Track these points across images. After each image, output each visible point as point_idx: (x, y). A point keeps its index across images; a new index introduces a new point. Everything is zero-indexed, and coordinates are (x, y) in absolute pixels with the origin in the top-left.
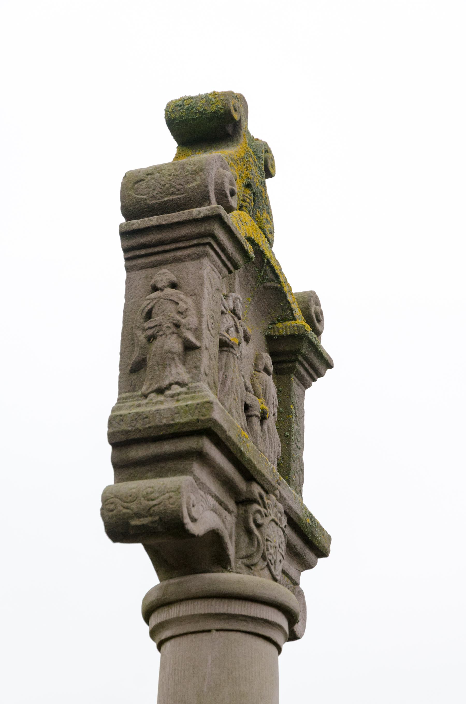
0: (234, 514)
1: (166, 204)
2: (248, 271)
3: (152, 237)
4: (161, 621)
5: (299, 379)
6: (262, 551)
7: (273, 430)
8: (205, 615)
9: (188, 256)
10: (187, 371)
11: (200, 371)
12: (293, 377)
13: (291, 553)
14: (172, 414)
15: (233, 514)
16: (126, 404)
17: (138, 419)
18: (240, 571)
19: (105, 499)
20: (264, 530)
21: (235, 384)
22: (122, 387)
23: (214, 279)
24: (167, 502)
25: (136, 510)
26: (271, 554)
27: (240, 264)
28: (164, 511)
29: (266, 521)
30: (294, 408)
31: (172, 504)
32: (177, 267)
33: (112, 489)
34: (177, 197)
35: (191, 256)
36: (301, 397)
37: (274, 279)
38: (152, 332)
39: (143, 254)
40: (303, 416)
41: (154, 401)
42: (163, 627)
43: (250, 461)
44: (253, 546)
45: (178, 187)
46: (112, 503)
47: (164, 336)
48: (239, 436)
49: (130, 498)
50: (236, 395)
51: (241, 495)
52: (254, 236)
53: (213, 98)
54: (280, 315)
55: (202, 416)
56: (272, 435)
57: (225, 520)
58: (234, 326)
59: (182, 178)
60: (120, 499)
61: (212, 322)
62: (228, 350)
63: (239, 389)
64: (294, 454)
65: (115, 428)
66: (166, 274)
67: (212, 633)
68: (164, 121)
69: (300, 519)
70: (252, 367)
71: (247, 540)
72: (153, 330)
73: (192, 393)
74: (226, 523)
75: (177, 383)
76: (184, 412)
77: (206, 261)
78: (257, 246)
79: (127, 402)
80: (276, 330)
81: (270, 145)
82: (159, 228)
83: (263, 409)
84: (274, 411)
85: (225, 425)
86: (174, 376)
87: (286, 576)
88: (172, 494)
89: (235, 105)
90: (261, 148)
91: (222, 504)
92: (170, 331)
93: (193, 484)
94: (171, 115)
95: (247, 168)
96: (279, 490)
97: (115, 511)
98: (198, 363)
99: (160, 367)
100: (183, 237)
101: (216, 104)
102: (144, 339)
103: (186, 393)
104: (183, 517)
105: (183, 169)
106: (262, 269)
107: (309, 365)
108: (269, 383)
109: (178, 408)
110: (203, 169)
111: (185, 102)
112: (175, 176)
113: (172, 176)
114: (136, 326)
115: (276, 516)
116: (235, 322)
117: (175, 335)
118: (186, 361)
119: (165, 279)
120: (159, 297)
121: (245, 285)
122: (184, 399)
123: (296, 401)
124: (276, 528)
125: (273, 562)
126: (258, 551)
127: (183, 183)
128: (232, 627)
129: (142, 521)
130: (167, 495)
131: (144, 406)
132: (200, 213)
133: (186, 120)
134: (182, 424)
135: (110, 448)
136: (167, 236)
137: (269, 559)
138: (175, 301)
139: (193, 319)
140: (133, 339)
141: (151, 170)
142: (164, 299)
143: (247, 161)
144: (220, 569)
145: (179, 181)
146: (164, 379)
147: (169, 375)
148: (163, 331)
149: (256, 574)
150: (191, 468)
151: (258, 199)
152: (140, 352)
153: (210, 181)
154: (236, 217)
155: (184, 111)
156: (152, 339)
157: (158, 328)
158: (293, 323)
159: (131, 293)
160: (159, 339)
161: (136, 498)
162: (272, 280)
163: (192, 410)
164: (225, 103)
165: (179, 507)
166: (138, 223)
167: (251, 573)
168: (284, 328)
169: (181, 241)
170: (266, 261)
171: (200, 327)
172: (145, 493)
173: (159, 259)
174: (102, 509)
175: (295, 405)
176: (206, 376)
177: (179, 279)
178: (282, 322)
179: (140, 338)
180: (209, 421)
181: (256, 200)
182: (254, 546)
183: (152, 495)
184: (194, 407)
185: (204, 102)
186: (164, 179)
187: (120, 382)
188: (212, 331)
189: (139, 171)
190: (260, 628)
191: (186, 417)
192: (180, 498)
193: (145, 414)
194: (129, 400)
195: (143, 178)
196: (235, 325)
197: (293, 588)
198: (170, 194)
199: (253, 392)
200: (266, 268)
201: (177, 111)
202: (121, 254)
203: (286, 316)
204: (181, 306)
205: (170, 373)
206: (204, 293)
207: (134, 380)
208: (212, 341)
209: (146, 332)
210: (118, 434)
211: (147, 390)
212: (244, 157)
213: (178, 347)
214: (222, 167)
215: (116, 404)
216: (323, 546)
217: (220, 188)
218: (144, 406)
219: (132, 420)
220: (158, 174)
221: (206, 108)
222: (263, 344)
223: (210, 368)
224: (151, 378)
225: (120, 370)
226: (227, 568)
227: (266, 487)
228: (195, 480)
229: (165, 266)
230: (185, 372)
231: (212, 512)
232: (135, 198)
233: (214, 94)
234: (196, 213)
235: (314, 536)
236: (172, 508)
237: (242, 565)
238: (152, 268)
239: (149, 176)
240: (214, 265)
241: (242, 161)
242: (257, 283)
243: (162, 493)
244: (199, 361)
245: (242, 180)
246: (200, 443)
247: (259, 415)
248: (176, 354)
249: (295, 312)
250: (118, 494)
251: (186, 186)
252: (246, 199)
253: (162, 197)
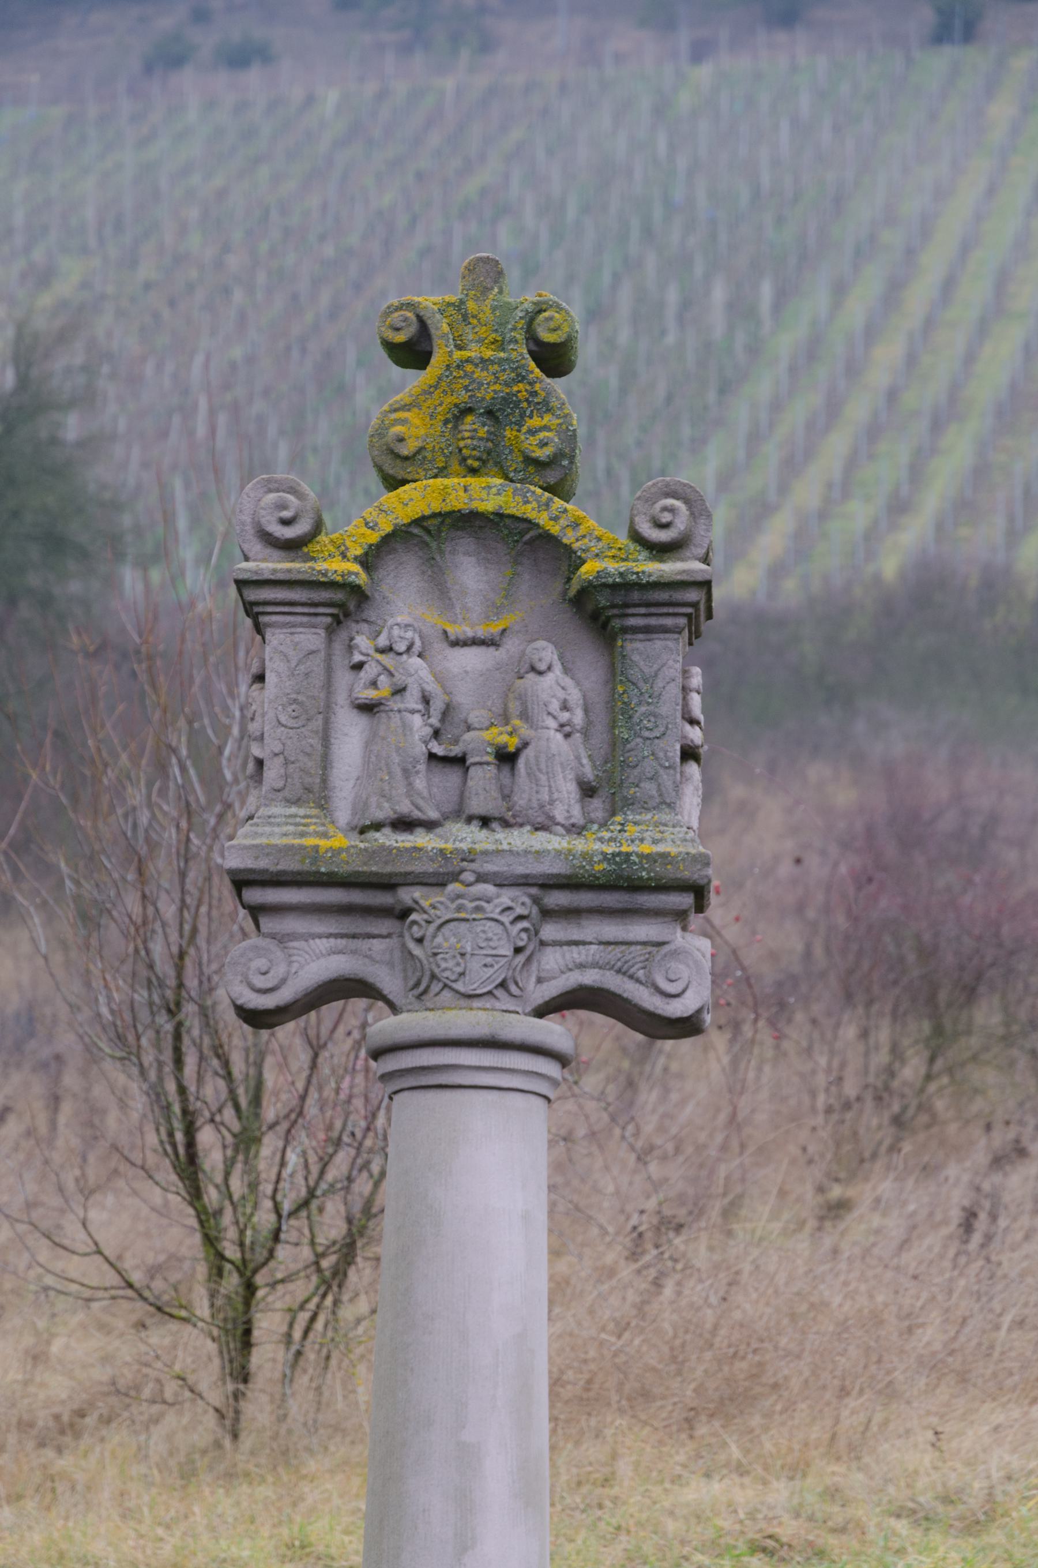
37: (529, 526)
162: (529, 529)
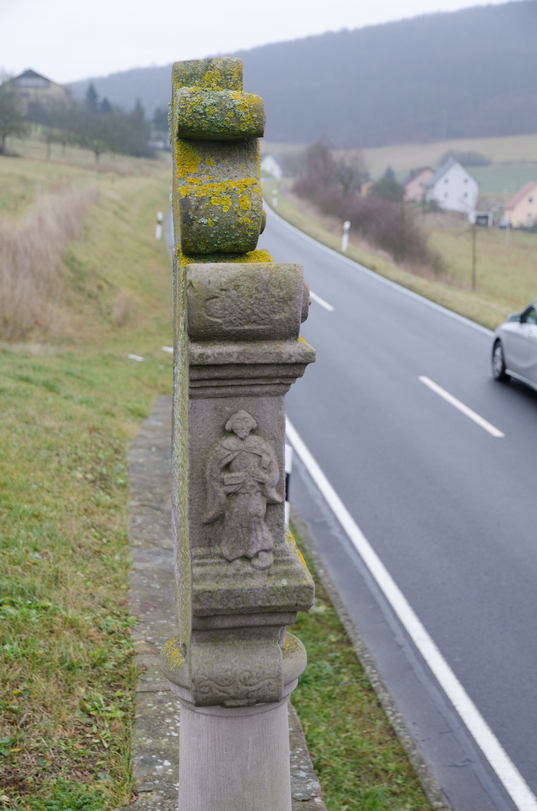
24: (267, 689)
31: (273, 691)
46: (206, 686)
55: (302, 601)
60: (215, 683)
66: (246, 420)
72: (236, 487)
88: (272, 681)
92: (255, 490)
99: (244, 529)
127: (268, 312)
130: (266, 681)
142: (247, 452)
145: (263, 307)
159: (197, 427)
164: (259, 124)
172: (243, 678)
185: (232, 116)
186: (244, 301)
193: (237, 593)
195: (217, 295)
205: (256, 538)
232: (208, 320)
239: (224, 293)
251: (271, 316)
253: (241, 324)
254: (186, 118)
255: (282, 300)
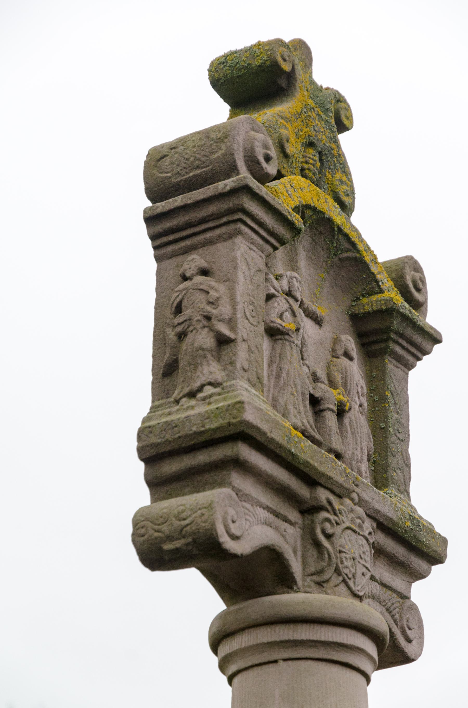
0: (299, 526)
1: (191, 180)
2: (316, 243)
3: (179, 219)
4: (225, 654)
5: (397, 361)
6: (335, 565)
7: (356, 423)
8: (268, 643)
9: (219, 236)
10: (222, 368)
11: (235, 367)
12: (387, 359)
13: (391, 563)
14: (202, 419)
15: (297, 526)
16: (156, 413)
17: (167, 428)
18: (309, 590)
19: (137, 523)
20: (335, 541)
21: (293, 376)
22: (155, 394)
23: (253, 259)
24: (199, 520)
25: (167, 532)
26: (347, 567)
27: (286, 238)
28: (197, 530)
29: (338, 530)
30: (392, 394)
31: (205, 522)
32: (209, 251)
33: (144, 511)
34: (202, 170)
35: (222, 236)
36: (402, 381)
37: (351, 248)
38: (181, 328)
39: (171, 240)
40: (407, 403)
41: (185, 407)
42: (228, 661)
43: (307, 463)
44: (323, 560)
45: (203, 159)
46: (142, 527)
47: (194, 332)
48: (287, 436)
49: (161, 519)
50: (294, 389)
51: (305, 502)
52: (313, 202)
53: (257, 50)
54: (364, 289)
55: (234, 418)
56: (356, 429)
57: (284, 533)
58: (290, 310)
59: (207, 149)
60: (151, 522)
61: (251, 309)
62: (283, 338)
63: (299, 382)
64: (393, 448)
65: (144, 441)
66: (195, 260)
67: (279, 663)
68: (208, 82)
69: (394, 523)
70: (329, 352)
71: (315, 553)
72: (183, 325)
73: (225, 393)
74: (287, 537)
75: (210, 384)
76: (214, 417)
77: (239, 240)
78: (321, 213)
79: (158, 411)
80: (360, 306)
81: (343, 93)
82: (185, 208)
83: (340, 401)
84: (360, 401)
85: (265, 426)
86: (206, 375)
87: (389, 589)
88: (204, 511)
89: (282, 54)
90: (329, 99)
91: (279, 515)
92: (201, 325)
93: (231, 497)
94: (214, 75)
95: (307, 124)
96: (356, 493)
97: (146, 536)
98: (234, 358)
99: (191, 367)
100: (211, 215)
101: (261, 56)
102: (174, 337)
103: (219, 394)
104: (217, 536)
105: (208, 137)
106: (334, 239)
107: (407, 342)
108: (350, 370)
109: (209, 412)
110: (228, 136)
111: (228, 58)
112: (199, 146)
113: (196, 148)
114: (166, 323)
115: (352, 521)
116: (290, 305)
117: (206, 329)
118: (221, 357)
119: (194, 265)
120: (187, 288)
121: (315, 260)
122: (216, 401)
123: (395, 386)
124: (354, 536)
125: (350, 576)
126: (329, 564)
127: (207, 154)
128: (300, 655)
129: (176, 544)
130: (199, 512)
131: (175, 413)
132: (226, 186)
133: (231, 78)
134: (213, 429)
135: (142, 465)
136: (194, 217)
137: (345, 574)
138: (205, 289)
139: (226, 309)
140: (164, 338)
141: (175, 143)
142: (194, 289)
143: (305, 116)
144: (286, 589)
145: (204, 152)
146: (195, 381)
147: (201, 376)
148: (193, 325)
149: (329, 591)
150: (229, 478)
151: (327, 158)
152: (171, 352)
153: (236, 149)
154: (284, 184)
155: (228, 68)
156: (183, 336)
157: (187, 323)
158: (380, 296)
160: (190, 335)
161: (168, 519)
162: (349, 250)
163: (223, 413)
164: (271, 54)
165: (212, 525)
166: (162, 206)
167: (322, 590)
168: (370, 303)
169: (209, 221)
170: (336, 229)
171: (234, 316)
172: (177, 513)
173: (189, 244)
174: (133, 535)
175: (392, 391)
176: (245, 371)
177: (211, 264)
178: (367, 297)
179: (170, 336)
180: (241, 423)
181: (324, 160)
182: (324, 560)
183: (183, 514)
184: (225, 409)
185: (248, 56)
186: (188, 152)
187: (153, 389)
188: (251, 319)
189: (162, 146)
190: (334, 653)
191: (216, 422)
192: (212, 515)
194: (160, 409)
195: (166, 153)
196: (290, 308)
197: (401, 603)
198: (195, 168)
199: (326, 382)
200: (338, 236)
201: (220, 69)
202: (149, 242)
203: (371, 289)
204: (212, 294)
205: (202, 372)
206: (238, 277)
207: (167, 385)
208: (253, 331)
209: (176, 328)
210: (148, 448)
211: (179, 395)
212: (301, 111)
213: (210, 342)
214: (253, 129)
215: (149, 413)
216: (434, 551)
217: (250, 154)
218: (175, 413)
219: (161, 431)
220: (182, 147)
221: (250, 62)
222: (346, 323)
223: (250, 362)
224: (183, 381)
225: (153, 375)
226: (293, 589)
227: (337, 490)
228: (235, 492)
229: (196, 251)
230: (219, 370)
231: (265, 526)
232: (159, 177)
233: (259, 44)
234: (221, 186)
235: (418, 540)
236: (205, 527)
237: (310, 582)
238: (184, 254)
239: (173, 150)
240: (252, 243)
241: (299, 117)
242: (330, 255)
243: (194, 511)
244: (235, 355)
245: (300, 139)
246: (235, 450)
247: (335, 409)
248: (208, 351)
249: (382, 283)
250: (149, 516)
251: (211, 157)
252: (309, 161)
253: (186, 173)
254: (213, 72)
255: (219, 140)
